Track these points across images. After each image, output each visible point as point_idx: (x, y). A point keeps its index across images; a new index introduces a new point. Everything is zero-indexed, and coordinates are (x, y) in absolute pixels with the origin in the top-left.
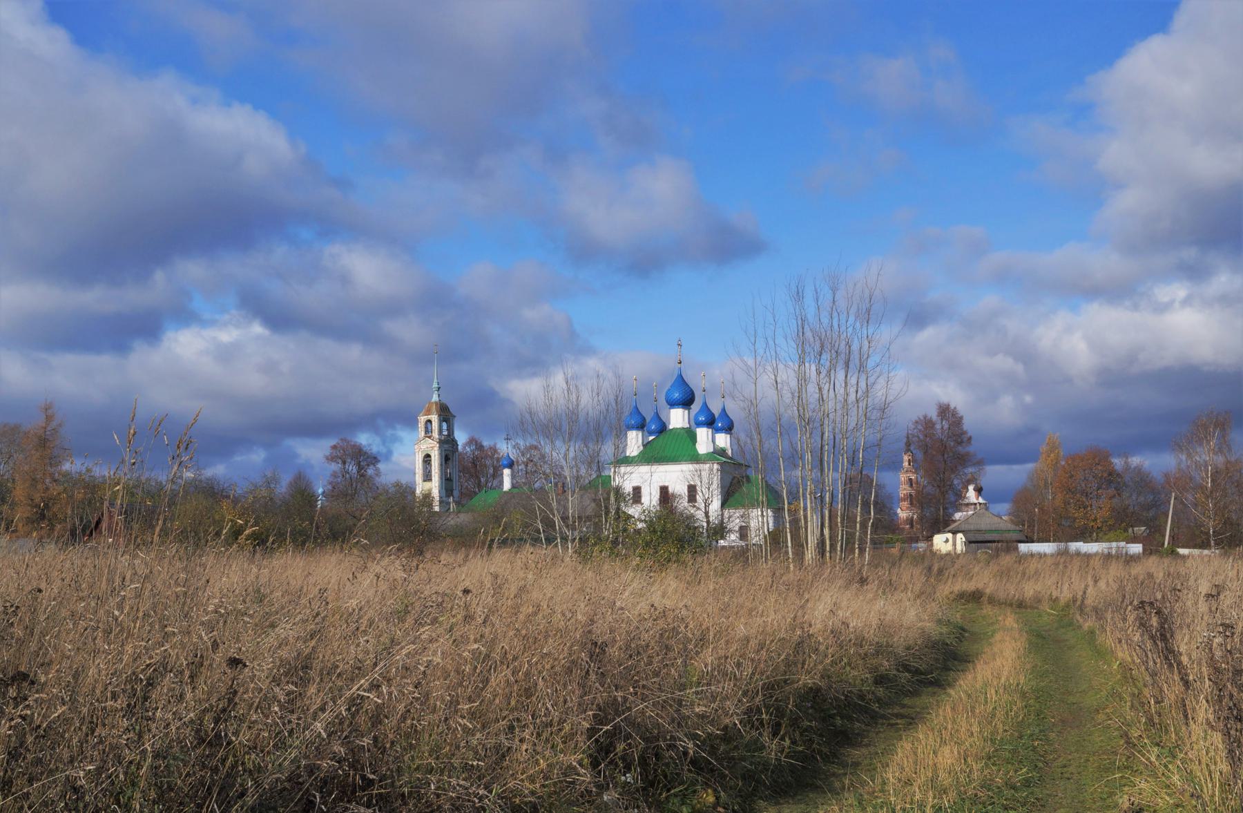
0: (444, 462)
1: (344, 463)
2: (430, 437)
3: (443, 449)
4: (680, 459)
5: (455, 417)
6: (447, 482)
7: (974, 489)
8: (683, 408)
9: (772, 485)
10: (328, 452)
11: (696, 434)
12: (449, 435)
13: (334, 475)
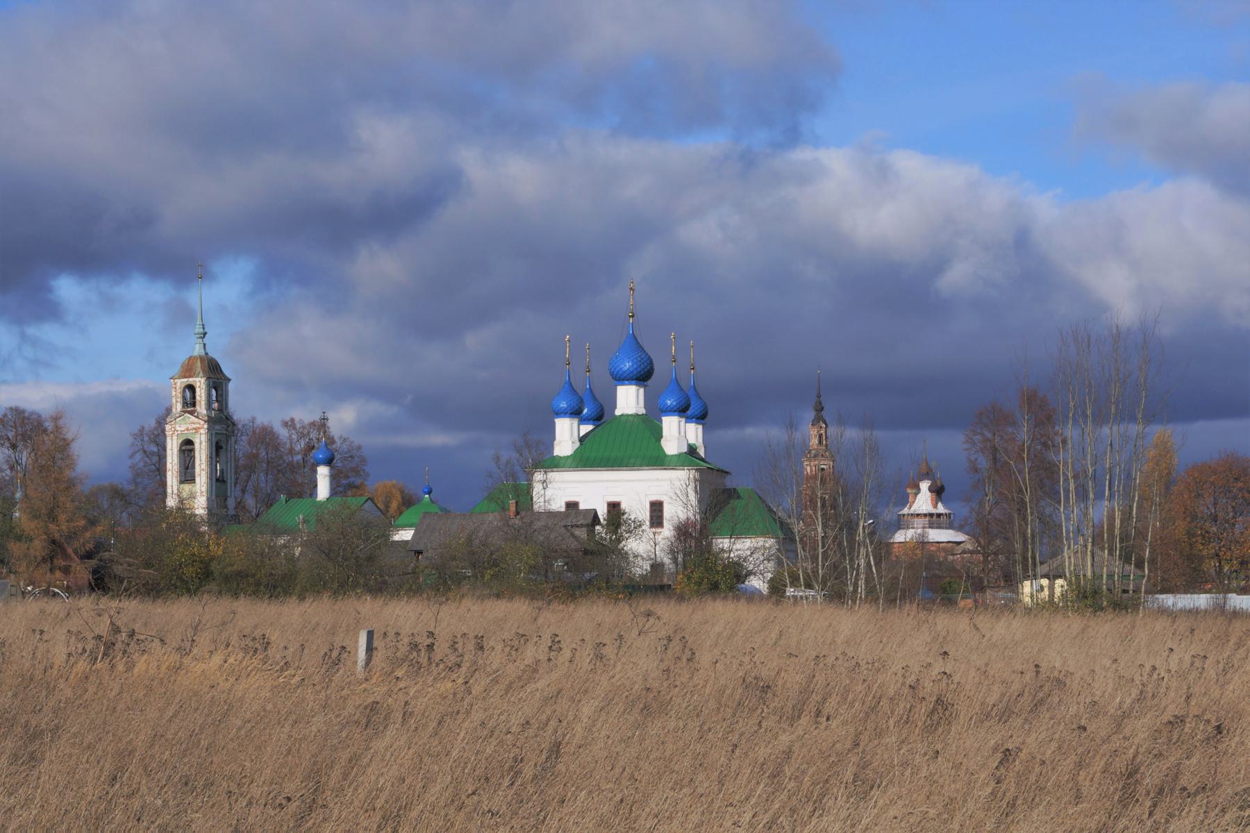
0: (214, 453)
2: (192, 413)
3: (214, 432)
4: (632, 461)
5: (229, 380)
6: (218, 482)
7: (930, 490)
8: (636, 385)
9: (296, 423)
11: (662, 428)
12: (220, 410)
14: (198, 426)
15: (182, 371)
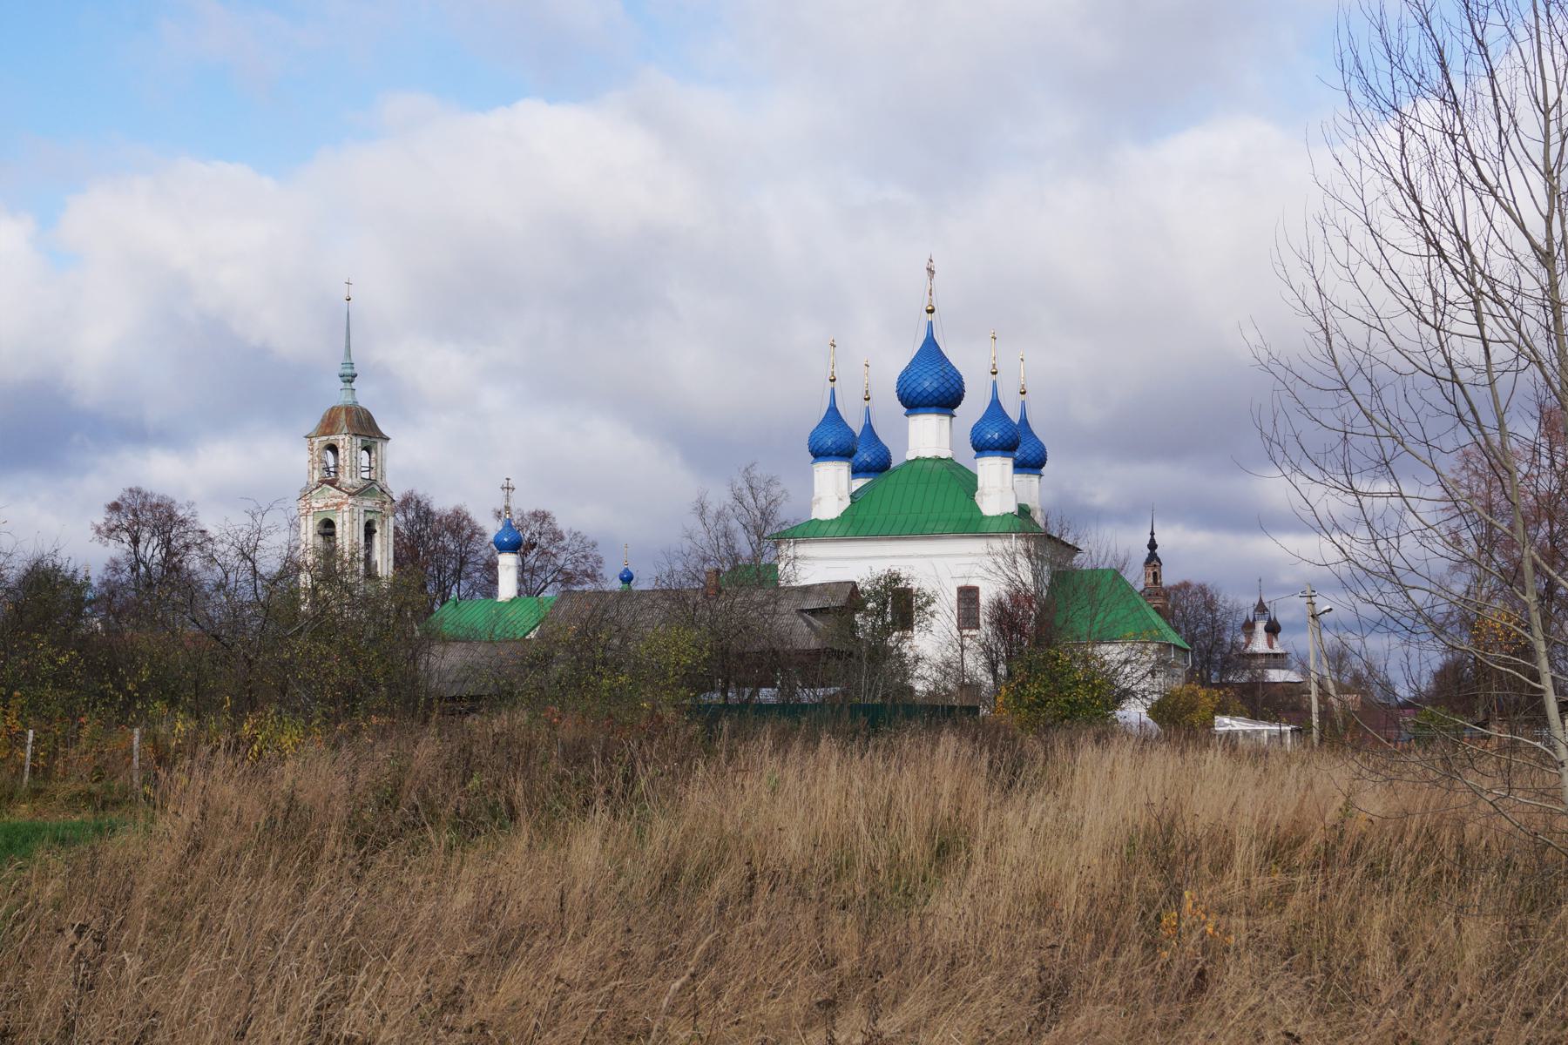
1: (135, 541)
8: (939, 413)
10: (100, 518)
13: (115, 566)
14: (340, 500)
15: (321, 427)
